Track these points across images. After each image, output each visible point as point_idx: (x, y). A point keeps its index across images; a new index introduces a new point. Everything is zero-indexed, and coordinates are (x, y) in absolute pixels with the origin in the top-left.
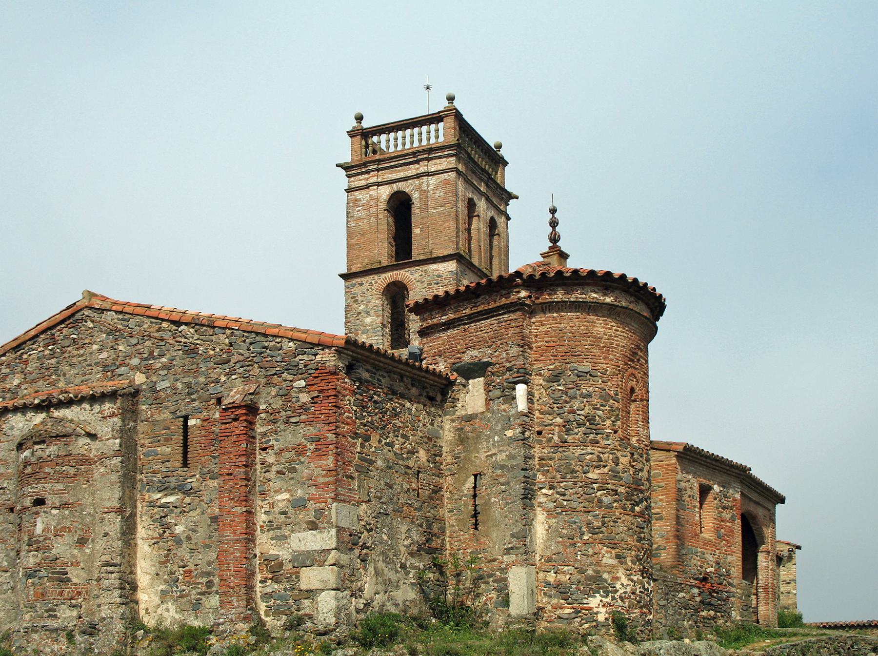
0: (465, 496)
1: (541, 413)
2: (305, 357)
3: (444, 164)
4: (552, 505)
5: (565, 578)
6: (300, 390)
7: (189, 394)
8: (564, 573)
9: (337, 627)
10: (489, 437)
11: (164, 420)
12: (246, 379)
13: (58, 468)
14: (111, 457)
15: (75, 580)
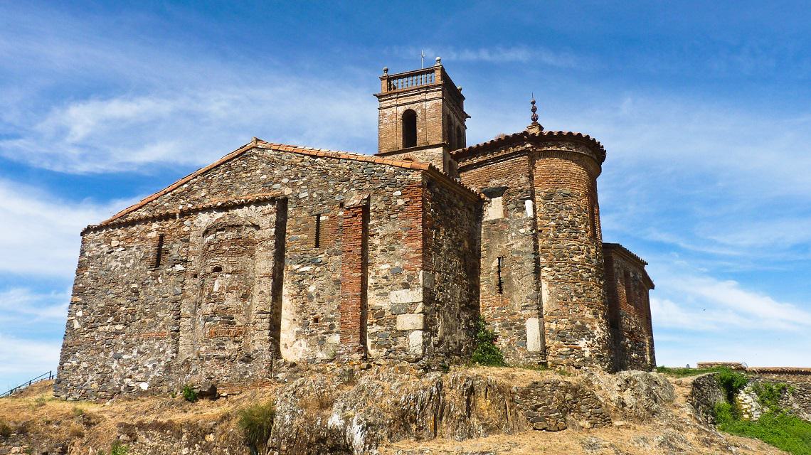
0: (492, 271)
1: (541, 219)
2: (401, 177)
3: (435, 95)
4: (551, 278)
5: (561, 327)
6: (398, 197)
7: (321, 200)
8: (562, 323)
9: (423, 357)
10: (508, 233)
11: (305, 217)
12: (361, 191)
13: (232, 247)
14: (268, 240)
15: (239, 323)
